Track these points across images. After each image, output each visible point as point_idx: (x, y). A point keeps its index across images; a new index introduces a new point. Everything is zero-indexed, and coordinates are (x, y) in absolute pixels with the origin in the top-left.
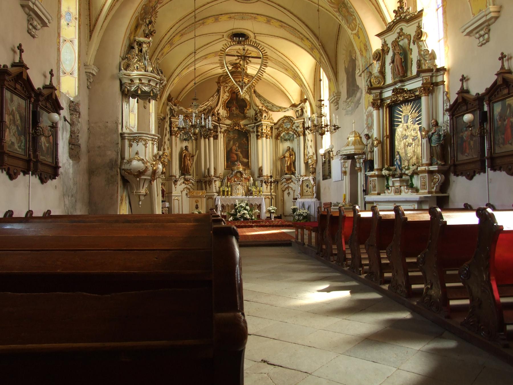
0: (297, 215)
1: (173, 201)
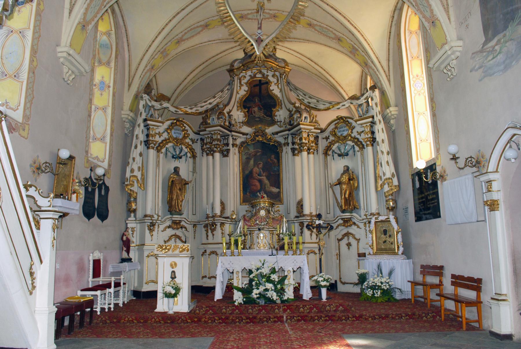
0: (368, 288)
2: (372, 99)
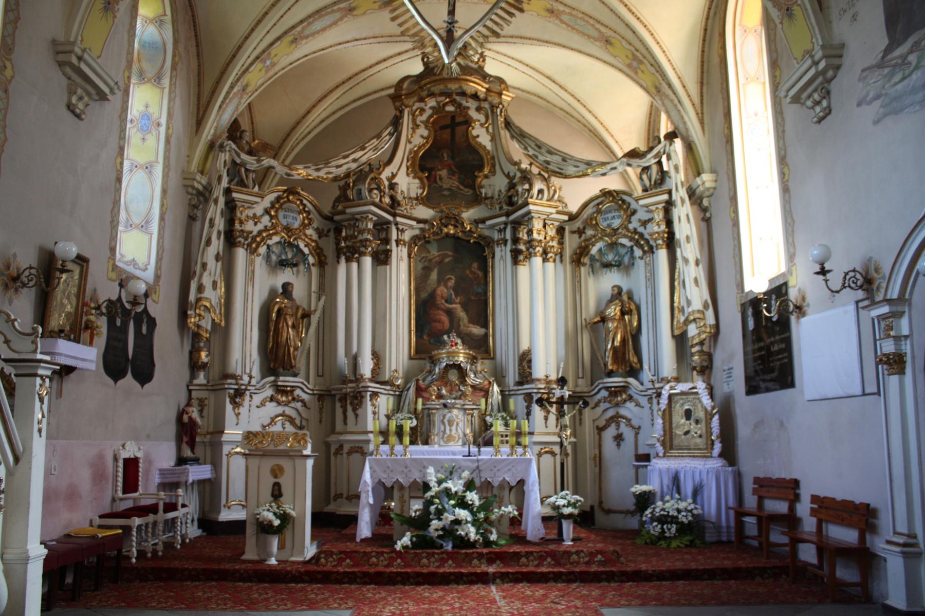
1: (225, 459)
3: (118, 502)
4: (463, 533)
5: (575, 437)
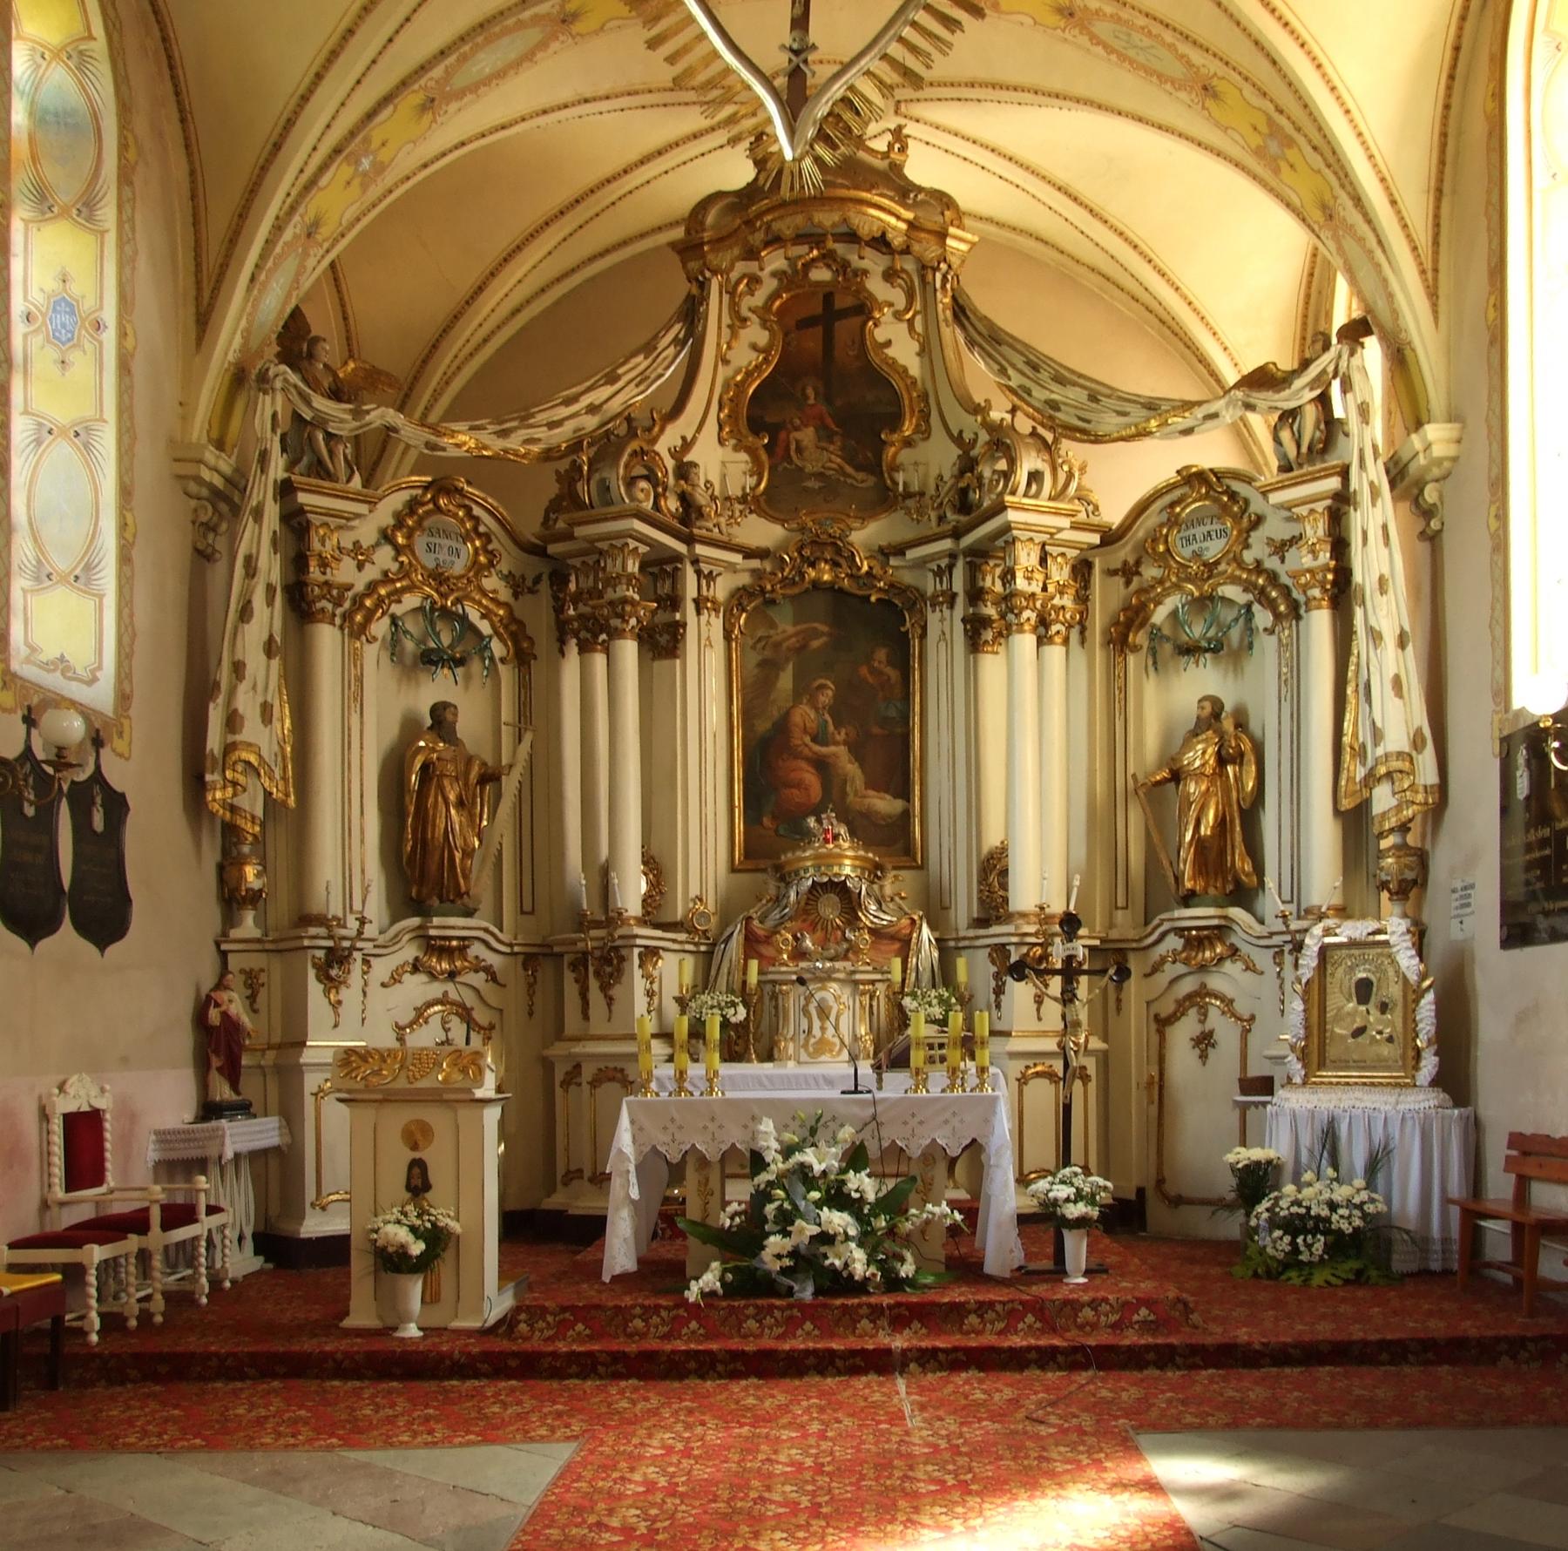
1: (309, 1102)
2: (1347, 387)
3: (55, 1209)
4: (837, 1263)
5: (1105, 1039)
